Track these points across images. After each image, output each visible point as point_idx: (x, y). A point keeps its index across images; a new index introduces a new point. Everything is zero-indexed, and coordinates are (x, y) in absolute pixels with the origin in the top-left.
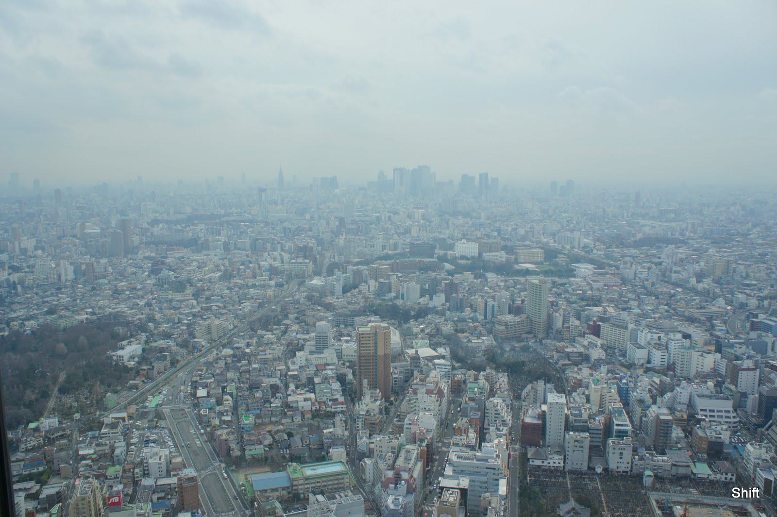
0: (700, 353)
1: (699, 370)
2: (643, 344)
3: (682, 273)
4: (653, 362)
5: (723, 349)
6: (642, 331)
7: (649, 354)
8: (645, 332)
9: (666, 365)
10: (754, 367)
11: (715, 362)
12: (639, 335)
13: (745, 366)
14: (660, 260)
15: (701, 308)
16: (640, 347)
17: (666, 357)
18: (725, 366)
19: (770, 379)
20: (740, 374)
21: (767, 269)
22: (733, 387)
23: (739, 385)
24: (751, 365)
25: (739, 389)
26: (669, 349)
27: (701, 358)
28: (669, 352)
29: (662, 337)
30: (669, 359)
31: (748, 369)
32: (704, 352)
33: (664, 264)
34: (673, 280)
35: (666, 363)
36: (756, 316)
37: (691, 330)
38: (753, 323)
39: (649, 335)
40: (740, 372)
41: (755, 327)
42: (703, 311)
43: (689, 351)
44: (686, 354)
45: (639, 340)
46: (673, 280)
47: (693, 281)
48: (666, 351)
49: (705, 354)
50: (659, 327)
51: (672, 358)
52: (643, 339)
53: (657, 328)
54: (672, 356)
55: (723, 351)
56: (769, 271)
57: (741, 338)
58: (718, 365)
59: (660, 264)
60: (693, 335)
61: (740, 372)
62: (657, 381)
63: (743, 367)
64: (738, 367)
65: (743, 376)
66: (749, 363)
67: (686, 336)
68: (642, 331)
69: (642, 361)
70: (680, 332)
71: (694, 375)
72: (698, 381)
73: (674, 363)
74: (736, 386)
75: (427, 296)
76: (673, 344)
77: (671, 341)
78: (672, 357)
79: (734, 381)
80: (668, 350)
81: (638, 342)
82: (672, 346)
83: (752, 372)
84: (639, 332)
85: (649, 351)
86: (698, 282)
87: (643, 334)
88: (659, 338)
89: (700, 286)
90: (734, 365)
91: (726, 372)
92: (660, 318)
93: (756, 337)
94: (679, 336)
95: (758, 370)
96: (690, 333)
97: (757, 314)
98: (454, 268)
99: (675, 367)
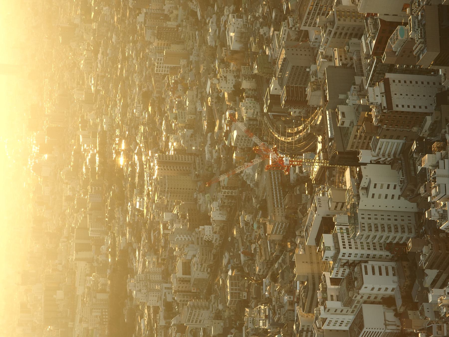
0: (361, 192)
1: (397, 192)
2: (350, 318)
3: (189, 258)
4: (389, 292)
5: (349, 149)
6: (324, 320)
7: (373, 303)
8: (323, 315)
9: (393, 264)
10: (382, 84)
11: (378, 163)
12: (331, 327)
13: (381, 100)
14: (162, 309)
15: (264, 208)
16: (359, 323)
17: (377, 264)
18: (385, 140)
19: (404, 51)
20: (400, 109)
21: (174, 90)
22: (429, 120)
23: (423, 110)
24: (379, 88)
25: (431, 109)
26: (358, 258)
27: (372, 190)
28: (364, 259)
29: (333, 275)
30: (381, 258)
31: (387, 93)
32: (359, 184)
33: (169, 299)
34: (205, 275)
35: (391, 265)
36: (275, 99)
37: (314, 218)
38: (290, 102)
39: (329, 304)
40: (395, 109)
41: (297, 98)
42: (269, 205)
43: (360, 217)
44: (366, 221)
45: (344, 328)
46: (205, 275)
47: (207, 231)
48: (363, 265)
49: (364, 183)
50: (311, 287)
51: (378, 253)
52: (341, 318)
53: (314, 290)
54: (372, 252)
55: (354, 149)
56: (180, 87)
57: (324, 121)
58: (384, 156)
59: (169, 307)
60: (323, 212)
61: (395, 109)
62: (431, 274)
63: (385, 104)
64: (384, 114)
65: (402, 101)
66: (376, 94)
67: (327, 225)
68: (324, 320)
69: (390, 316)
70: (318, 240)
71: (411, 200)
72: (422, 190)
73: (389, 247)
74: (428, 114)
75: (214, 16)
76: (347, 251)
77: (340, 256)
78: (375, 252)
79: (417, 118)
80: (360, 262)
81: (347, 328)
82: (350, 252)
83: (393, 88)
84: (325, 327)
85: (365, 302)
86: (206, 220)
87: (329, 317)
88: (334, 281)
89: (216, 215)
90: (380, 121)
91: (398, 138)
92: (291, 292)
93: (319, 93)
94: (327, 239)
95: (387, 75)
96: (321, 219)
97: (272, 96)
98: (123, 141)
99: (398, 243)
